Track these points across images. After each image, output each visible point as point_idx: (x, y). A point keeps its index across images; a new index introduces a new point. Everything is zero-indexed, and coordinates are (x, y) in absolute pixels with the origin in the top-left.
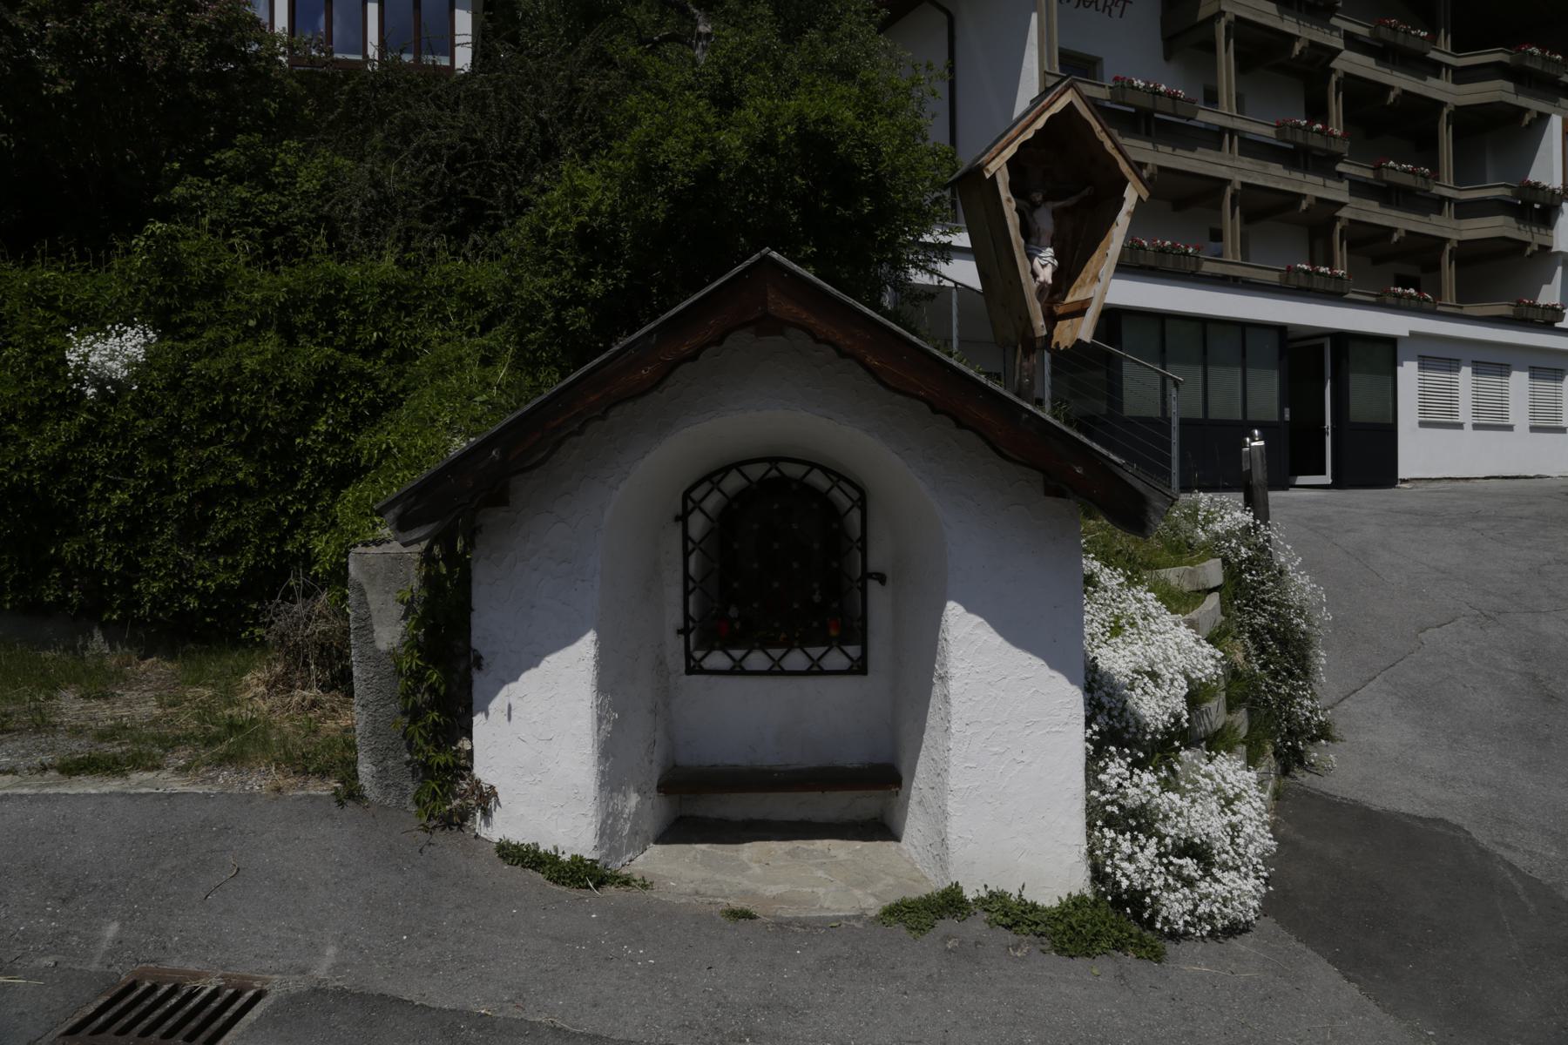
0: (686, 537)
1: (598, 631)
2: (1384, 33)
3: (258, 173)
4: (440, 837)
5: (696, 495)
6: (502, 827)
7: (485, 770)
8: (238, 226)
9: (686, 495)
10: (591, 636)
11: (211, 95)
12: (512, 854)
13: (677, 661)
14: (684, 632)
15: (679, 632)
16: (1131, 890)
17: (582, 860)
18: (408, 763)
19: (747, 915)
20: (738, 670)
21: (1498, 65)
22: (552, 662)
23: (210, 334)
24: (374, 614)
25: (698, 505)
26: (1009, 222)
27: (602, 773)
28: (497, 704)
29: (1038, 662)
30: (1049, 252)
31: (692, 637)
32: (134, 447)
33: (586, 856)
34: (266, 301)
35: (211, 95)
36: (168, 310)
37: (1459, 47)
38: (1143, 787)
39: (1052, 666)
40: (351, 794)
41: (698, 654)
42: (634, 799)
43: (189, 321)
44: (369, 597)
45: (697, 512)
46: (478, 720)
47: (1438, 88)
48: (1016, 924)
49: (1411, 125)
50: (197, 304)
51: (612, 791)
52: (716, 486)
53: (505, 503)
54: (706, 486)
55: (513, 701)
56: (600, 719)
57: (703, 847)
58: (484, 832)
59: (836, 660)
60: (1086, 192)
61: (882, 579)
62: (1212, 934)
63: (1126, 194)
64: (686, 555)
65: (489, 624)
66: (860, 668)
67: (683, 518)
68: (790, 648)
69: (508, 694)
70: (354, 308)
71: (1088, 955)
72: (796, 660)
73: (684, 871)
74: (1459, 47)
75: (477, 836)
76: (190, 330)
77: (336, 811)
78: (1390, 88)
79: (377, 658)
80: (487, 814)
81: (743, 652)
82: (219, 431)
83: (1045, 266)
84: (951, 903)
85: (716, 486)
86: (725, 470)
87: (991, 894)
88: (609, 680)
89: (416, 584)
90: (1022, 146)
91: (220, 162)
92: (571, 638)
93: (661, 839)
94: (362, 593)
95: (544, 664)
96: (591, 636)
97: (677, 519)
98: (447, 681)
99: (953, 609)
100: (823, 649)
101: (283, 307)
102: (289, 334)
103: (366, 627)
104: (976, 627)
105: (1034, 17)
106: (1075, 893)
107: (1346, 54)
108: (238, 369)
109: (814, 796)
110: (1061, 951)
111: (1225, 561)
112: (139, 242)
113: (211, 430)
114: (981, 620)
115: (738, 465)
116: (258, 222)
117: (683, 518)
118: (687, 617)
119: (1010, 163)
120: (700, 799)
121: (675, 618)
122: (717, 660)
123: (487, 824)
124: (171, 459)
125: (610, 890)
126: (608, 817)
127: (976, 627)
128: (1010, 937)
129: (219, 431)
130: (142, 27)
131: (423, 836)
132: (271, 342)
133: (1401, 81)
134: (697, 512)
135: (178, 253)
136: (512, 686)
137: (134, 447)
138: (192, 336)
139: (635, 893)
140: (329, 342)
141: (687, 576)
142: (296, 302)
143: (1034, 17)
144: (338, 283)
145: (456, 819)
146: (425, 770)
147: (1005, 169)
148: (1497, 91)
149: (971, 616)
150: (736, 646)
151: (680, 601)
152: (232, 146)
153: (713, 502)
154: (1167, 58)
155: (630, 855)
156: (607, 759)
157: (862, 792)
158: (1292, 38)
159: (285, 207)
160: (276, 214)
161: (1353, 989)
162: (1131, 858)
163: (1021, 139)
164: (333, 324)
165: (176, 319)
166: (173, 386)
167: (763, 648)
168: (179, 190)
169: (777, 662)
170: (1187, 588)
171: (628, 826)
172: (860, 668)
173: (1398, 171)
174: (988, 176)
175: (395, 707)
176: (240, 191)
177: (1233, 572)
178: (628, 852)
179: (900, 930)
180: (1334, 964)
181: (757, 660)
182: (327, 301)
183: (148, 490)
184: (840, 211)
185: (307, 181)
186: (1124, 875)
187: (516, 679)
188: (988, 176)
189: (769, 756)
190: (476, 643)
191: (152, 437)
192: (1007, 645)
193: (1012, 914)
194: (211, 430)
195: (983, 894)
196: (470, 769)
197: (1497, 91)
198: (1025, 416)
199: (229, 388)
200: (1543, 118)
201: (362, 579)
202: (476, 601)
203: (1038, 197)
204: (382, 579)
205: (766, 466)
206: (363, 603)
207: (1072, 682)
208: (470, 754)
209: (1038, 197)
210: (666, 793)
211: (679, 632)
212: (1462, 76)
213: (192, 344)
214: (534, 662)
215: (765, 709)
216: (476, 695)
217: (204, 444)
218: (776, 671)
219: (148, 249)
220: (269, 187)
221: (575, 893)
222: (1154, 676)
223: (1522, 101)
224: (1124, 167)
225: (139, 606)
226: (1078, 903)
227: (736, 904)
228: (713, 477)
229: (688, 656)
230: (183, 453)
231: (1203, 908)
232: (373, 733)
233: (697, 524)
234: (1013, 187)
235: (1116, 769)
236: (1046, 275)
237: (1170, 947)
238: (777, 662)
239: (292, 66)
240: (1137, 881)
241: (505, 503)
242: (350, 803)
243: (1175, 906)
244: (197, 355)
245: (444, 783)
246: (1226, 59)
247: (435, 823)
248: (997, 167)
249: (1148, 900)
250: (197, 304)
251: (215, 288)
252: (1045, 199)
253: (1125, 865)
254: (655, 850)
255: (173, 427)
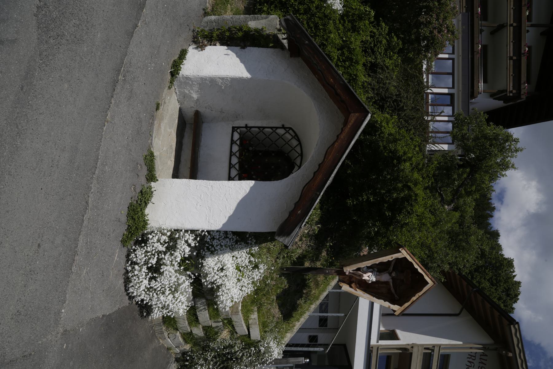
0: (277, 128)
1: (251, 78)
3: (389, 47)
4: (191, 34)
5: (291, 131)
6: (192, 52)
7: (209, 48)
8: (374, 40)
9: (291, 128)
10: (249, 76)
11: (413, 37)
12: (183, 54)
13: (236, 124)
14: (246, 127)
15: (246, 125)
16: (148, 239)
17: (180, 70)
18: (214, 28)
19: (157, 108)
20: (233, 142)
22: (242, 66)
23: (340, 26)
25: (287, 132)
26: (384, 258)
27: (206, 79)
28: (230, 52)
29: (231, 212)
30: (374, 280)
31: (244, 129)
32: (307, 5)
33: (181, 72)
34: (351, 42)
35: (413, 37)
36: (348, 16)
38: (183, 250)
39: (230, 217)
40: (206, 14)
41: (238, 131)
42: (195, 96)
43: (345, 22)
44: (264, 20)
45: (285, 131)
46: (226, 47)
48: (142, 194)
50: (350, 24)
51: (200, 84)
52: (293, 137)
53: (291, 56)
54: (293, 134)
55: (231, 56)
56: (223, 79)
57: (177, 121)
58: (191, 47)
60: (396, 296)
62: (127, 272)
63: (396, 306)
64: (271, 128)
65: (254, 52)
67: (283, 127)
68: (239, 158)
70: (349, 67)
71: (128, 214)
72: (235, 160)
73: (171, 107)
75: (190, 45)
76: (342, 22)
77: (202, 7)
79: (246, 21)
80: (197, 48)
81: (238, 156)
82: (312, 28)
83: (369, 277)
84: (151, 177)
85: (293, 137)
86: (299, 140)
87: (152, 192)
88: (236, 81)
89: (268, 32)
90: (411, 263)
91: (393, 38)
92: (249, 71)
93: (180, 110)
94: (266, 18)
95: (241, 64)
96: (249, 76)
97: (283, 125)
98: (236, 39)
100: (238, 169)
101: (349, 48)
102: (341, 48)
103: (255, 19)
104: (245, 190)
105: (461, 343)
106: (149, 222)
108: (330, 32)
109: (189, 165)
110: (131, 205)
111: (260, 341)
112: (368, 9)
113: (312, 25)
114: (248, 191)
115: (300, 144)
116: (375, 45)
117: (283, 127)
118: (251, 127)
119: (405, 258)
120: (191, 127)
121: (251, 124)
122: (236, 136)
123: (193, 48)
124: (303, 14)
125: (169, 77)
126: (192, 81)
127: (245, 190)
128: (138, 190)
129: (312, 28)
130: (432, 16)
131: (192, 28)
132: (338, 41)
134: (285, 131)
135: (365, 20)
137: (307, 5)
138: (340, 22)
139: (168, 84)
140: (339, 59)
141: (264, 128)
142: (351, 51)
143: (461, 343)
144: (357, 63)
145: (196, 40)
146: (211, 31)
147: (403, 256)
149: (249, 189)
150: (240, 142)
151: (256, 126)
152: (398, 40)
153: (288, 136)
155: (178, 92)
156: (210, 82)
157: (190, 166)
159: (380, 53)
160: (378, 51)
161: (100, 315)
162: (159, 241)
163: (414, 263)
164: (344, 61)
165: (345, 18)
166: (326, 16)
167: (239, 162)
168: (383, 24)
169: (235, 154)
170: (250, 322)
171: (187, 92)
174: (400, 249)
176: (384, 41)
177: (255, 344)
178: (179, 91)
179: (146, 153)
180: (109, 315)
181: (235, 148)
182: (351, 59)
183: (294, 8)
184: (386, 205)
185: (388, 62)
186: (153, 236)
187: (237, 57)
188: (400, 249)
189: (203, 152)
190: (248, 48)
191: (310, 9)
192: (238, 201)
193: (145, 197)
194: (312, 25)
195: (153, 190)
196: (210, 45)
198: (318, 193)
199: (325, 30)
201: (269, 19)
202: (261, 49)
203: (394, 274)
204: (270, 23)
205: (300, 152)
206: (262, 18)
207: (224, 225)
208: (215, 45)
209: (394, 274)
210: (195, 113)
211: (246, 125)
213: (338, 22)
215: (219, 144)
216: (232, 47)
217: (308, 23)
218: (231, 154)
219: (366, 11)
220: (386, 50)
221: (170, 65)
222: (222, 269)
224: (407, 305)
225: (260, 5)
226: (145, 223)
228: (296, 137)
229: (238, 128)
230: (305, 17)
231: (136, 267)
232: (224, 20)
233: (281, 131)
234: (397, 259)
235: (190, 238)
236: (366, 277)
237: (125, 250)
238: (234, 166)
239: (426, 93)
240: (150, 241)
241: (291, 56)
242: (203, 12)
243: (140, 255)
244: (335, 23)
247: (195, 34)
248: (404, 253)
249: (143, 245)
250: (350, 24)
251: (355, 29)
252: (393, 278)
253: (157, 237)
254: (178, 106)
255: (313, 15)
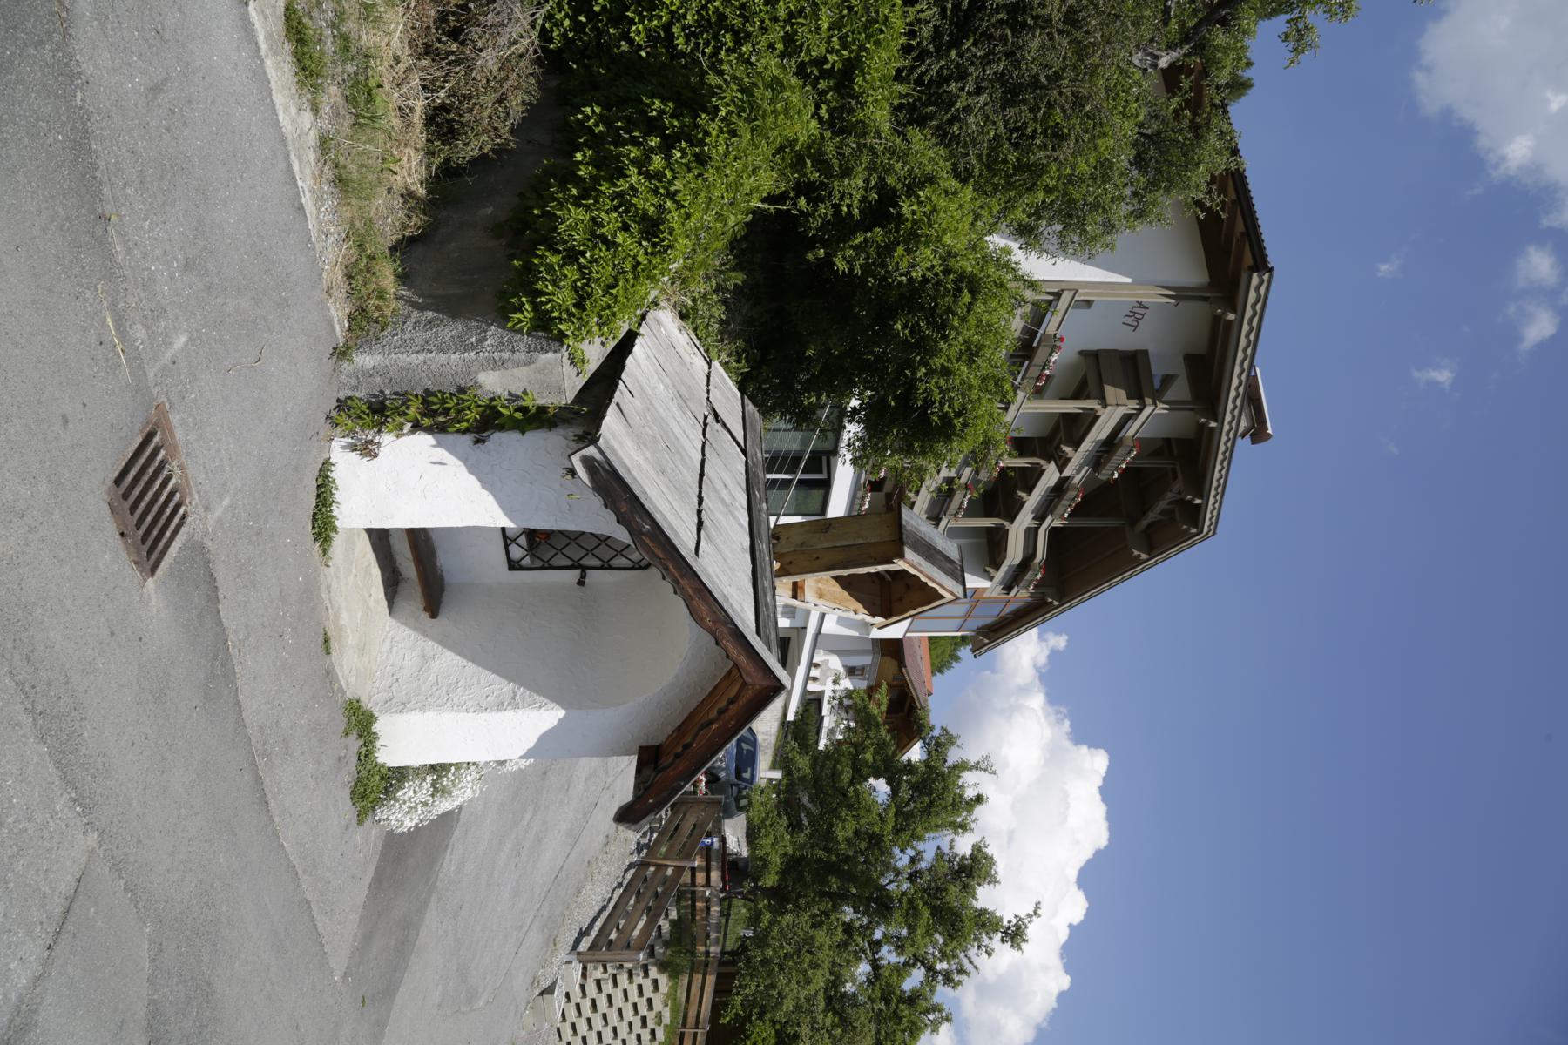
2: (1071, 494)
6: (345, 464)
21: (1034, 555)
22: (488, 499)
24: (509, 372)
28: (442, 454)
37: (1053, 532)
40: (341, 353)
47: (1025, 519)
49: (1000, 498)
59: (517, 552)
61: (581, 583)
66: (513, 565)
69: (455, 467)
74: (1053, 532)
78: (1029, 492)
80: (353, 448)
99: (561, 713)
103: (498, 365)
105: (1129, 280)
107: (1057, 475)
133: (1033, 500)
136: (464, 469)
143: (1129, 280)
148: (1015, 552)
154: (1081, 352)
158: (1076, 446)
169: (514, 540)
172: (513, 565)
173: (961, 499)
175: (429, 384)
187: (471, 471)
197: (1015, 552)
200: (991, 578)
212: (1031, 534)
214: (485, 484)
223: (1004, 568)
227: (334, 644)
245: (373, 413)
246: (1071, 406)
